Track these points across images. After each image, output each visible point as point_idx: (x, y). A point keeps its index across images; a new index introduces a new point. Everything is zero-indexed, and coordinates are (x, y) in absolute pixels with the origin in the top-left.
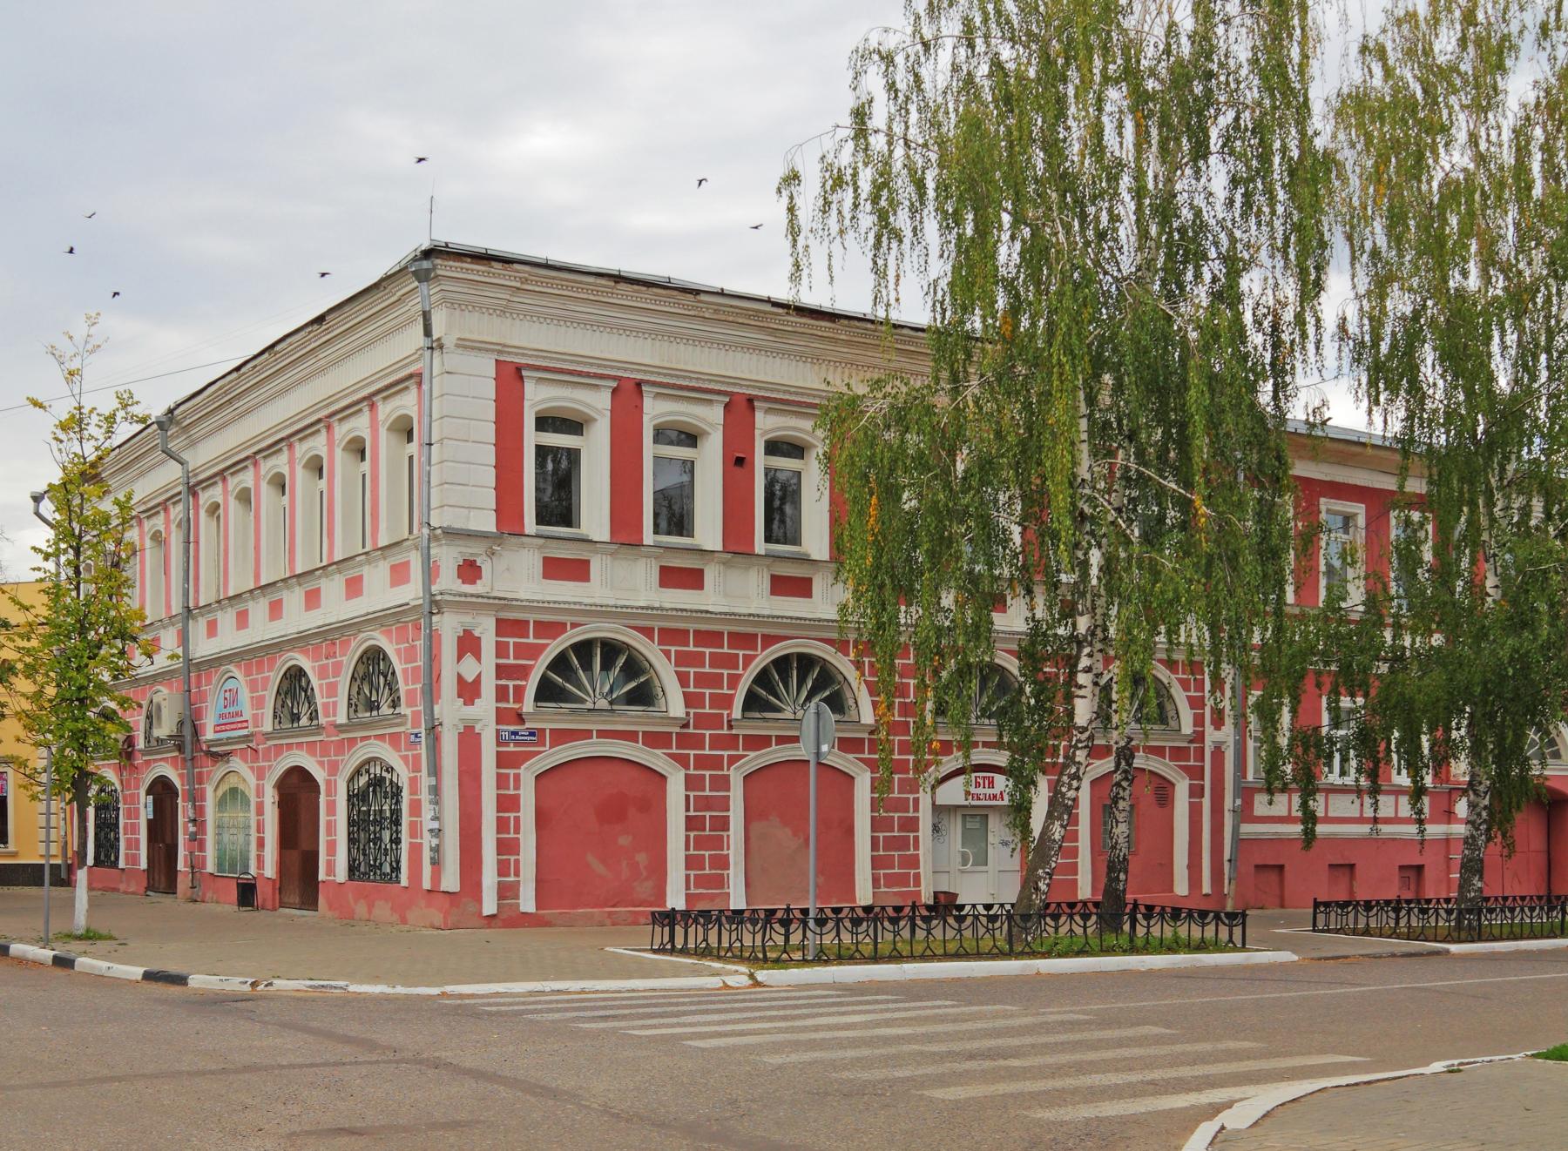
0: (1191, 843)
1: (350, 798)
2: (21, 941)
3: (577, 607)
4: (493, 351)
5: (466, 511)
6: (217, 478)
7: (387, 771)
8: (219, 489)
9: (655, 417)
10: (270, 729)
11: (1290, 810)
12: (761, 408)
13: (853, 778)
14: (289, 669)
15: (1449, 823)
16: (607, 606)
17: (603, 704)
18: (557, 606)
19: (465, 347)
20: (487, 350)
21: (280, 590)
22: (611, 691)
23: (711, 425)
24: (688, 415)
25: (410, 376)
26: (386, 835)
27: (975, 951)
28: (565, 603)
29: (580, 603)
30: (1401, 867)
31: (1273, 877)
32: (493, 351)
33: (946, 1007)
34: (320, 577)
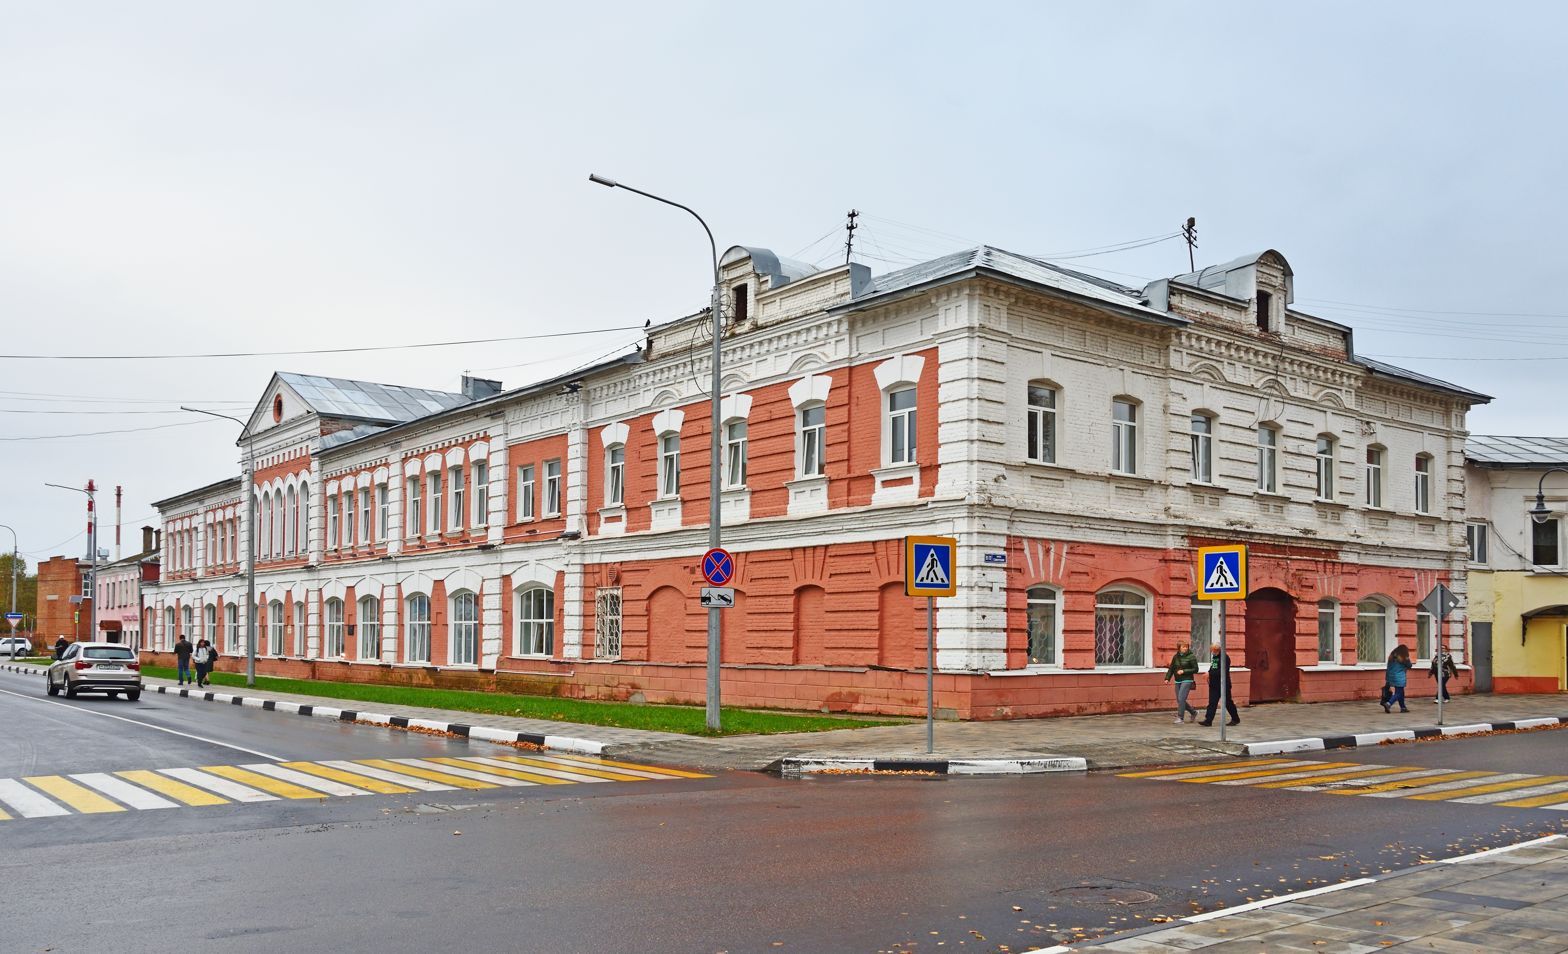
0: (60, 805)
11: (851, 353)
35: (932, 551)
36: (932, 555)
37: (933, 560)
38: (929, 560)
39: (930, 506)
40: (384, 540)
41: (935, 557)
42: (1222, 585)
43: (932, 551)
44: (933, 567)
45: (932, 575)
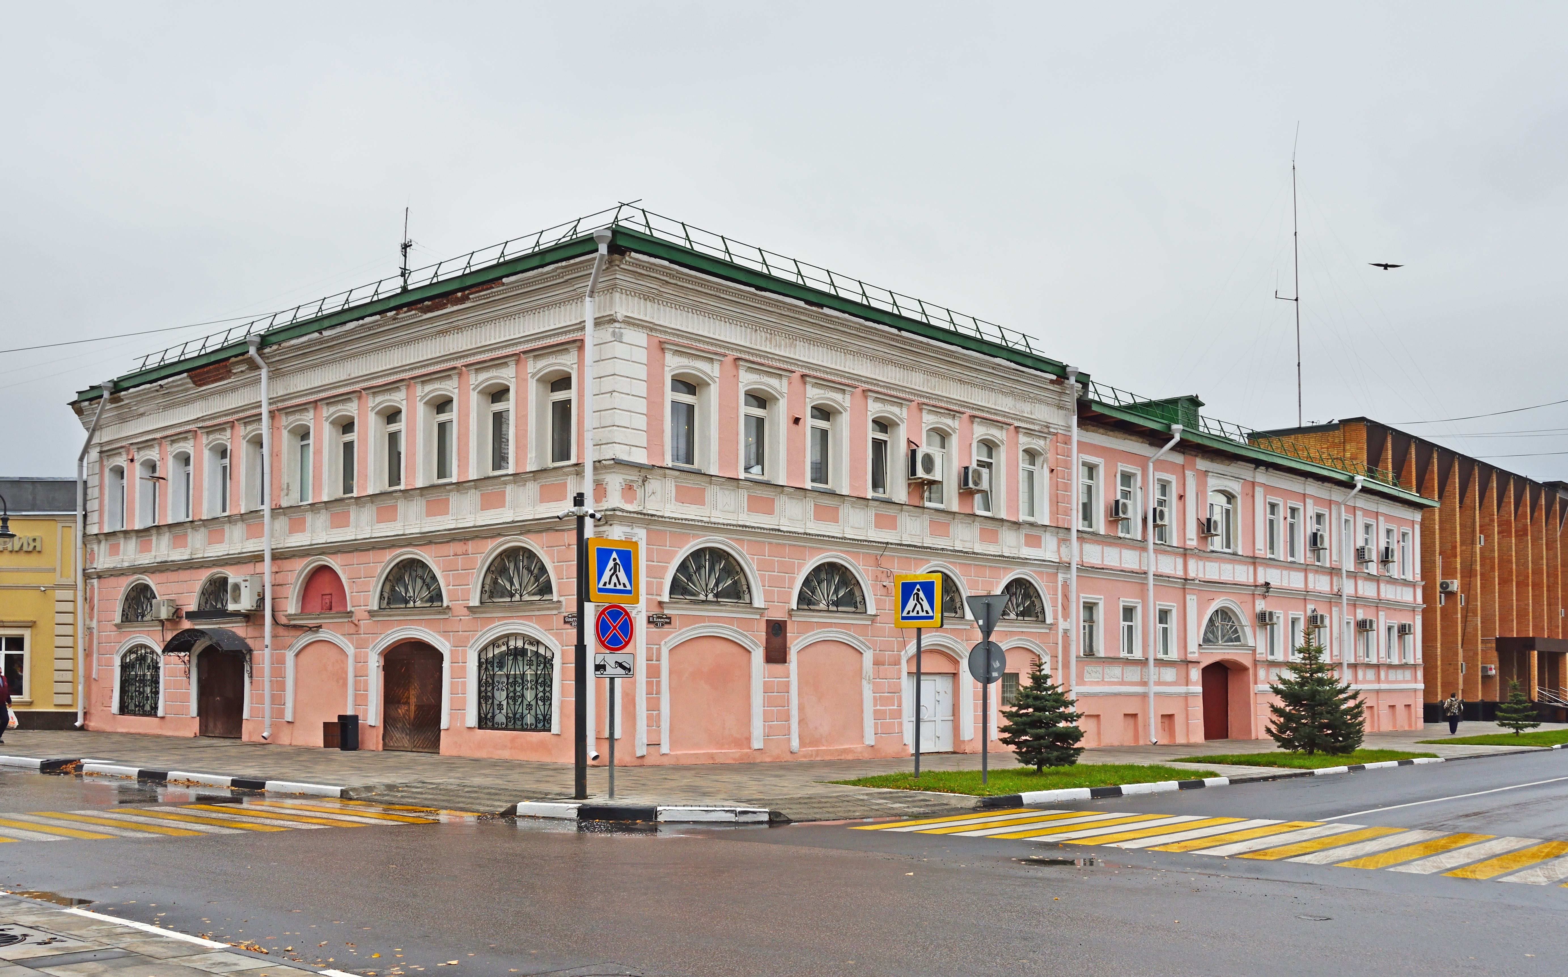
1: (480, 665)
2: (1393, 768)
3: (700, 524)
4: (646, 327)
5: (628, 447)
6: (311, 405)
7: (531, 644)
8: (311, 414)
9: (747, 385)
10: (376, 608)
12: (810, 383)
13: (749, 652)
14: (401, 561)
15: (1187, 685)
16: (719, 524)
17: (711, 597)
18: (687, 522)
19: (629, 323)
20: (643, 327)
21: (397, 499)
22: (717, 584)
23: (780, 393)
24: (765, 384)
25: (575, 341)
26: (148, 690)
27: (1380, 694)
28: (692, 520)
29: (702, 521)
30: (1162, 716)
31: (1131, 721)
32: (646, 327)
33: (818, 816)
34: (450, 491)
35: (614, 555)
36: (614, 560)
37: (616, 564)
38: (611, 564)
39: (972, 801)
40: (525, 662)
41: (618, 561)
42: (918, 612)
43: (614, 555)
44: (615, 571)
45: (614, 579)
